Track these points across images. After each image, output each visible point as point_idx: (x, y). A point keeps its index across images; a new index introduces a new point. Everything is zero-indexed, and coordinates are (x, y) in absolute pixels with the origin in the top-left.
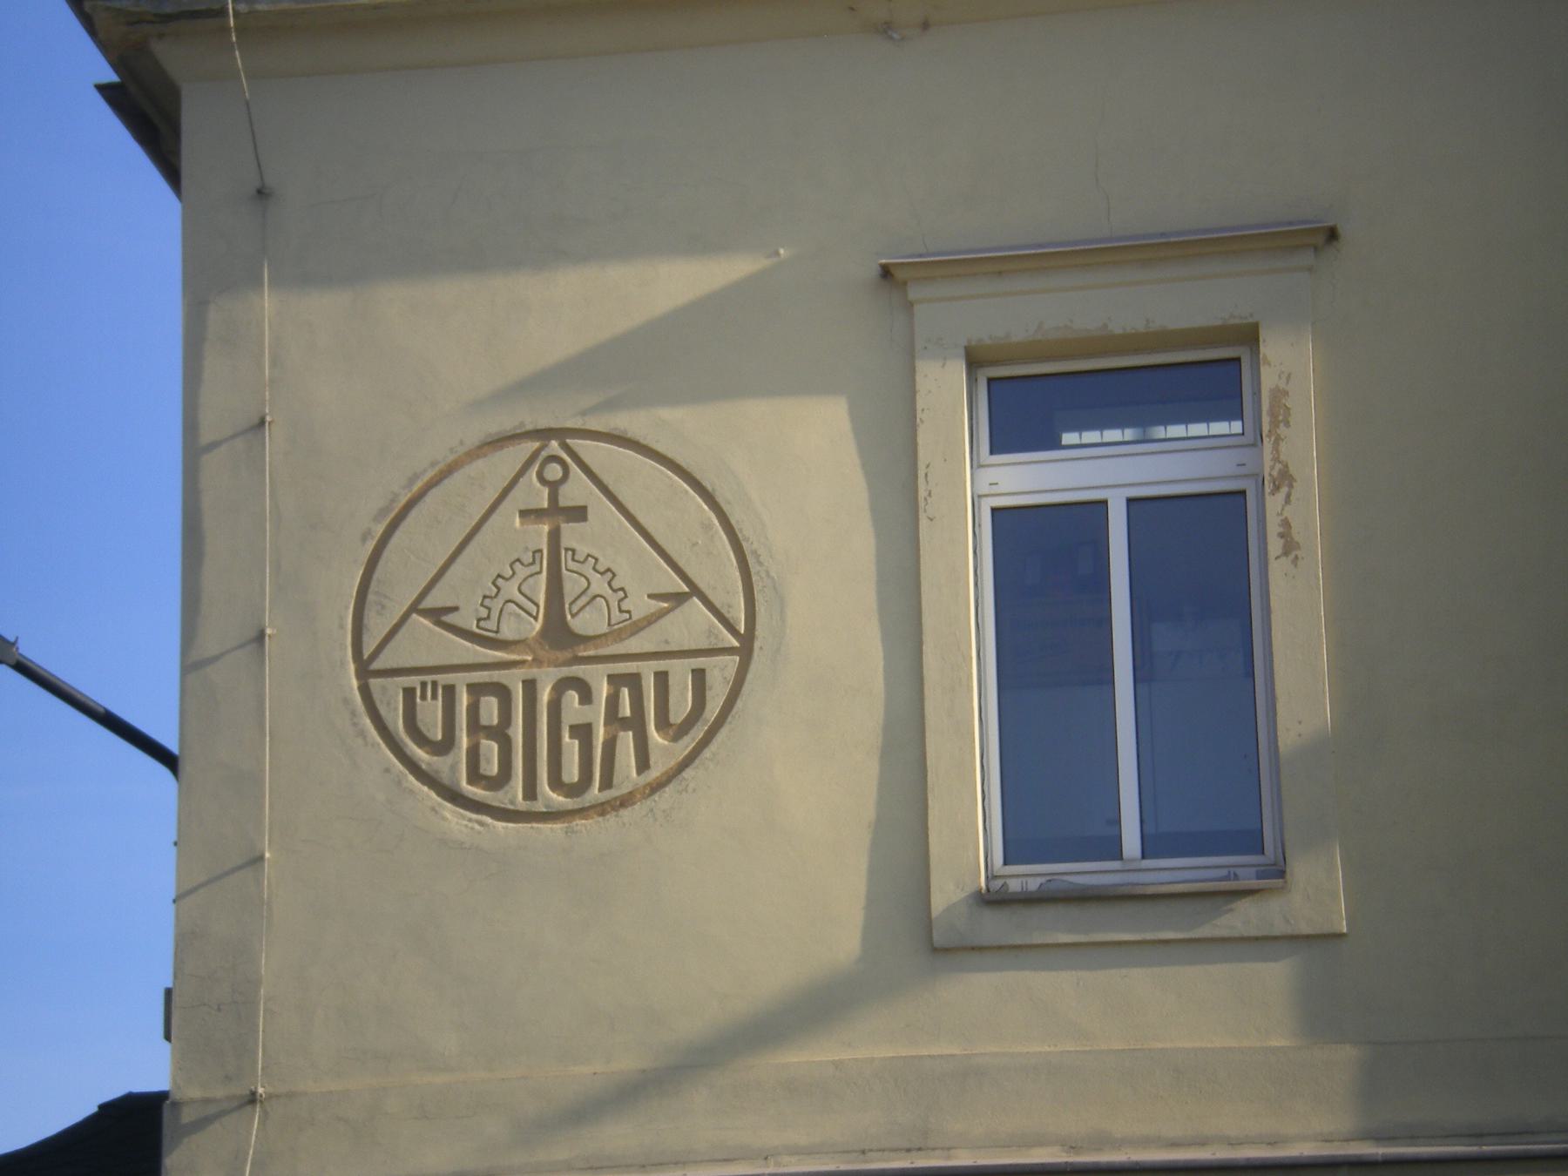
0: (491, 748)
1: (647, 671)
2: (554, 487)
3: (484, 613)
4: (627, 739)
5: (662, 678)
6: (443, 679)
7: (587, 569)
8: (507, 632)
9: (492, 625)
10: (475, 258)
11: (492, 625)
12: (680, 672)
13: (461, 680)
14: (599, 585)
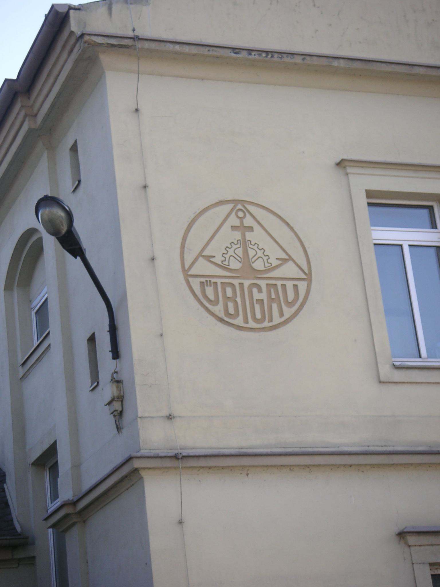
0: (231, 305)
1: (279, 283)
2: (241, 219)
3: (224, 259)
4: (275, 307)
5: (284, 286)
6: (213, 280)
7: (255, 247)
8: (232, 267)
9: (226, 263)
10: (148, 565)
11: (226, 263)
12: (289, 285)
13: (219, 281)
14: (260, 253)
